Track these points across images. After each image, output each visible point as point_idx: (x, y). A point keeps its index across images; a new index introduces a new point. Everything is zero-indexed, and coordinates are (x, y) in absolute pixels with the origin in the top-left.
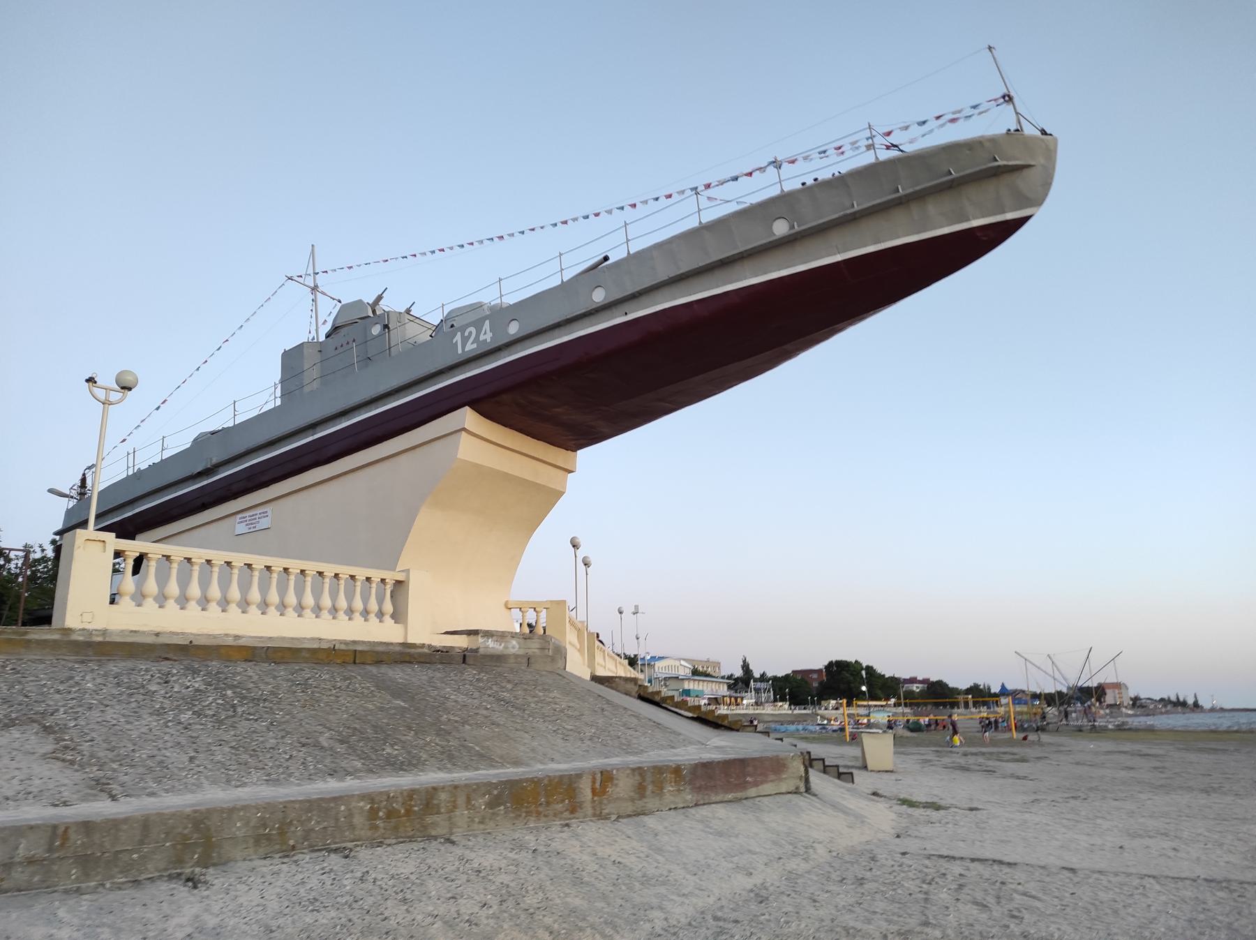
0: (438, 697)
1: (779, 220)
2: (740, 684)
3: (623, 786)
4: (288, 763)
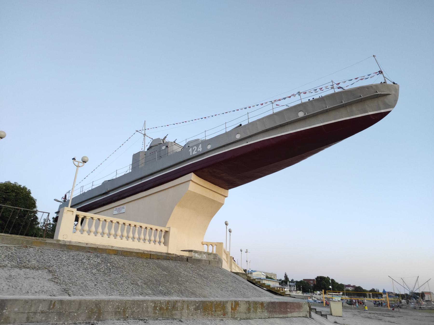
0: (178, 272)
1: (301, 112)
2: (284, 283)
3: (242, 308)
4: (127, 289)
